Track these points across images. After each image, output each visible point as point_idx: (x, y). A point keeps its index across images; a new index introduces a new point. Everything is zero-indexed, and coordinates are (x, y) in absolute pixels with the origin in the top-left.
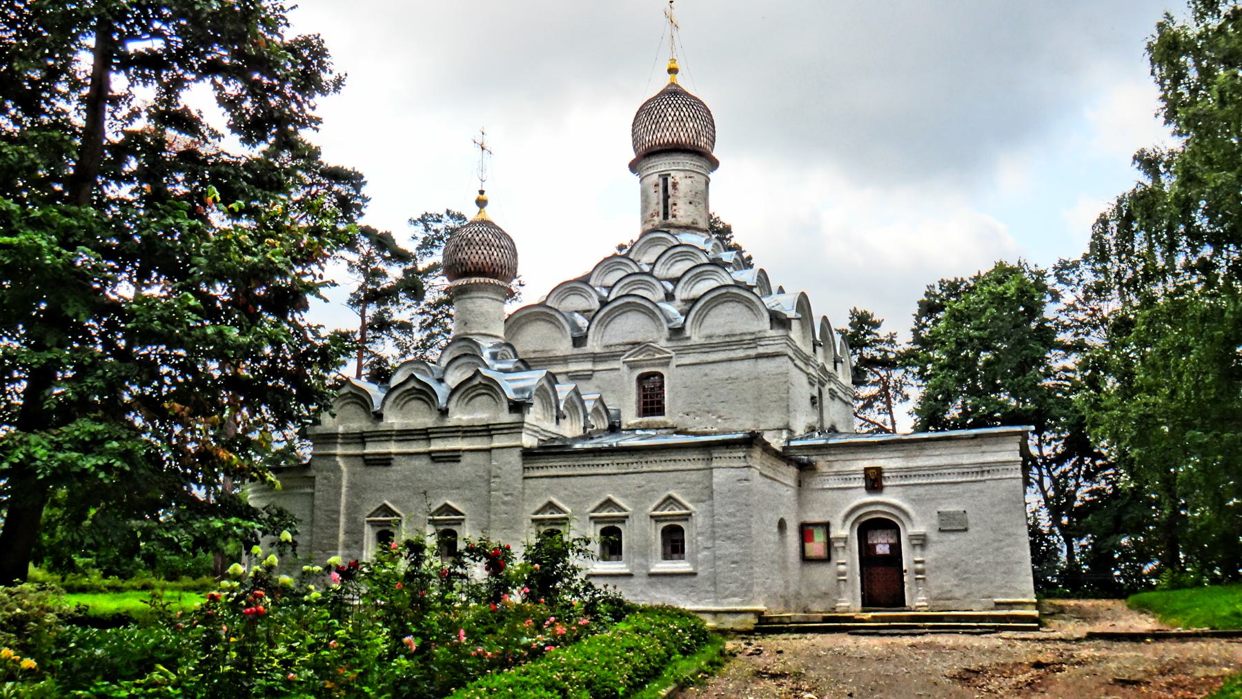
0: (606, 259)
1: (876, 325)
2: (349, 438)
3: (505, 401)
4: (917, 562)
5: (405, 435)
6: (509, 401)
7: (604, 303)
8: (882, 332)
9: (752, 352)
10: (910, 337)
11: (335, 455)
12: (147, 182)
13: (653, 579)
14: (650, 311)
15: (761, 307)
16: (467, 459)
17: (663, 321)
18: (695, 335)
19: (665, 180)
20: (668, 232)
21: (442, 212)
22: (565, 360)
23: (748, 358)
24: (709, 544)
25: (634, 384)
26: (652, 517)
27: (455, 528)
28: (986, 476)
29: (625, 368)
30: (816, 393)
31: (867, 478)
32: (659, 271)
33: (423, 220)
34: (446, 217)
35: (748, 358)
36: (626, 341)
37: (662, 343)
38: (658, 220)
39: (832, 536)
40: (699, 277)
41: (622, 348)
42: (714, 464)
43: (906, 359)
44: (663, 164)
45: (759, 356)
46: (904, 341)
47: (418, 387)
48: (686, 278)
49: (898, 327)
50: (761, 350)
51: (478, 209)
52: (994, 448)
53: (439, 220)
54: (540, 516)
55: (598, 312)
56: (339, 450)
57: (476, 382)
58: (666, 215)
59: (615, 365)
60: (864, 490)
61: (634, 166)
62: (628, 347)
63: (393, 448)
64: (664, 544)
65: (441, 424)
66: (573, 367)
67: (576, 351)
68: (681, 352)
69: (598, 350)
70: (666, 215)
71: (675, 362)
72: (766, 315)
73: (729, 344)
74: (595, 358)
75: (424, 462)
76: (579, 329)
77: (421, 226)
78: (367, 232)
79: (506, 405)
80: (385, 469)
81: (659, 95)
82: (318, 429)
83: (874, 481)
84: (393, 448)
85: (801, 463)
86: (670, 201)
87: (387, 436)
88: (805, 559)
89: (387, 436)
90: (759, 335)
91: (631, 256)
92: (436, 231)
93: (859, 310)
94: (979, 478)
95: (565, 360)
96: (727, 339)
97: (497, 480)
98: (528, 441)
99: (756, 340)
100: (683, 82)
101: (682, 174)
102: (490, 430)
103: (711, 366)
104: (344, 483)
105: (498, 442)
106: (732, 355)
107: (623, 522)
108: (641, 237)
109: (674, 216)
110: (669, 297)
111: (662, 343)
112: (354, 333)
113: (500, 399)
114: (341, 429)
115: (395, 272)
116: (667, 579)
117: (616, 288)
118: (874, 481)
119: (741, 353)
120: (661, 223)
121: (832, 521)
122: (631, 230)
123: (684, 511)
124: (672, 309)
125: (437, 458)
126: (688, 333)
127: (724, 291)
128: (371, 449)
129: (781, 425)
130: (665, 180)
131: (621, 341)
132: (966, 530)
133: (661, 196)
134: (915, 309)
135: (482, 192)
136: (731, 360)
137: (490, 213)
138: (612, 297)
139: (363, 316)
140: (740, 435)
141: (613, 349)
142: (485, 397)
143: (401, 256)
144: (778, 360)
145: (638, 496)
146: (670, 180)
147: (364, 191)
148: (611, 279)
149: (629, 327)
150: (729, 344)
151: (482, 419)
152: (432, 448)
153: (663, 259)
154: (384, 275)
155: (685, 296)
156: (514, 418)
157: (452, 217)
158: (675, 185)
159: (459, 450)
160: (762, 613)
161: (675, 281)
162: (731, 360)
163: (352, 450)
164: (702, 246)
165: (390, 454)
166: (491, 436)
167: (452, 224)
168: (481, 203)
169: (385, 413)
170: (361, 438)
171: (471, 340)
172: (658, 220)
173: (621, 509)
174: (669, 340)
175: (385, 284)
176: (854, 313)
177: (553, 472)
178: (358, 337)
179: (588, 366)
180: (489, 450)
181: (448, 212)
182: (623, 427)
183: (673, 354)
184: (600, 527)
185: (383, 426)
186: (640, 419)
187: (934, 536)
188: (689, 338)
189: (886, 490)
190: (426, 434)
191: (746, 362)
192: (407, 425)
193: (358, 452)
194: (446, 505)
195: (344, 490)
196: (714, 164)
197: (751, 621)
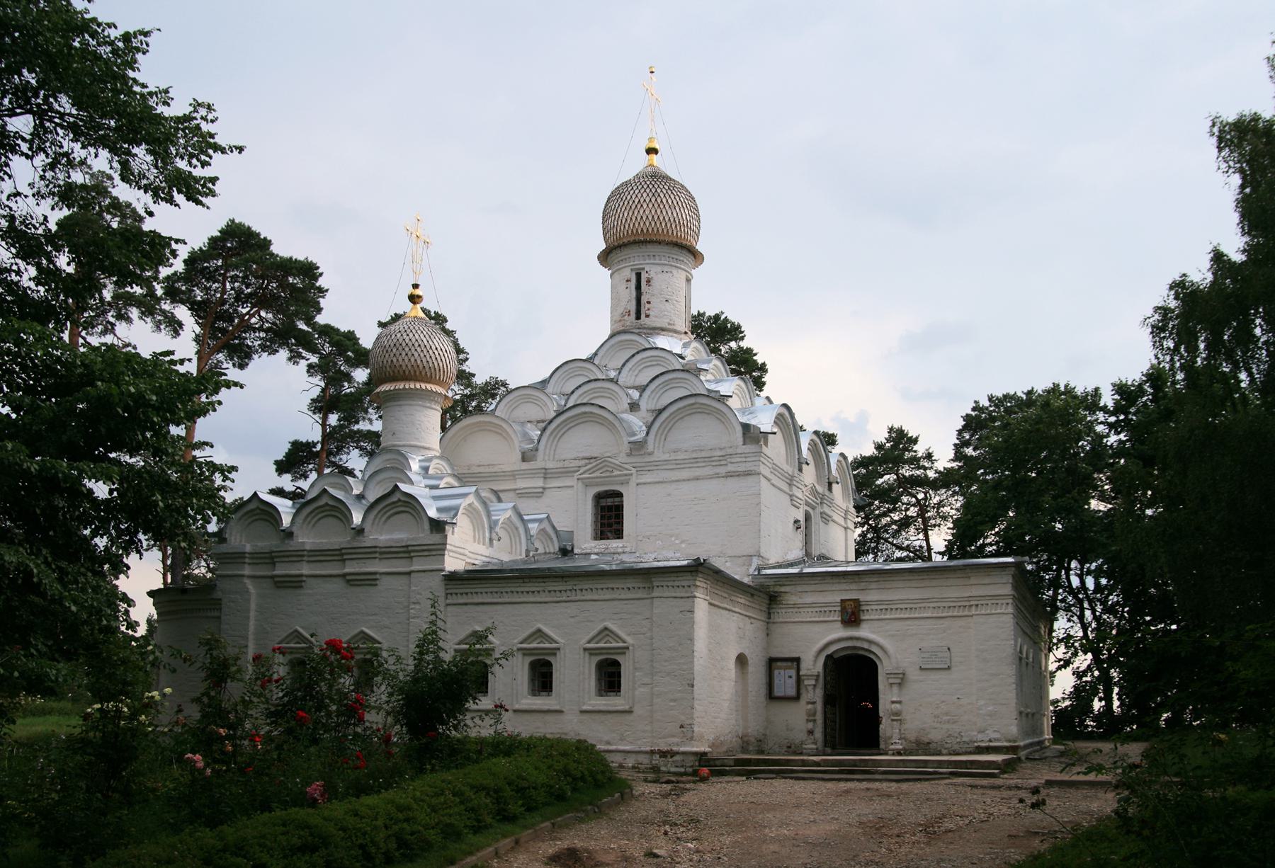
0: (566, 363)
1: (915, 441)
3: (425, 520)
4: (893, 702)
5: (319, 555)
6: (430, 519)
8: (920, 449)
9: (722, 470)
10: (951, 455)
11: (243, 576)
12: (1254, 336)
13: (585, 717)
14: (607, 421)
15: (733, 420)
16: (385, 582)
17: (623, 433)
19: (639, 276)
20: (639, 334)
22: (513, 475)
23: (717, 476)
24: (646, 680)
26: (585, 649)
30: (801, 518)
31: (843, 611)
32: (625, 378)
36: (582, 455)
40: (667, 386)
41: (577, 463)
42: (655, 594)
43: (946, 480)
44: (635, 259)
45: (730, 475)
46: (944, 459)
47: (331, 503)
48: (653, 386)
49: (939, 444)
50: (731, 468)
52: (987, 581)
55: (551, 422)
56: (247, 571)
57: (394, 498)
58: (638, 317)
59: (568, 482)
60: (839, 625)
61: (605, 258)
62: (583, 462)
63: (305, 570)
64: (599, 680)
65: (356, 544)
66: (521, 484)
67: (525, 466)
68: (640, 469)
69: (550, 465)
70: (638, 317)
71: (634, 480)
72: (739, 429)
74: (546, 474)
75: (338, 585)
76: (531, 441)
78: (327, 331)
79: (427, 526)
80: (298, 591)
82: (224, 548)
83: (852, 615)
84: (305, 570)
85: (767, 595)
86: (644, 299)
87: (299, 556)
88: (771, 696)
90: (730, 451)
91: (596, 361)
93: (896, 426)
94: (966, 613)
95: (513, 475)
96: (694, 455)
97: (417, 607)
99: (725, 458)
101: (659, 269)
102: (272, 558)
103: (674, 486)
104: (253, 606)
106: (698, 472)
107: (555, 654)
109: (647, 316)
110: (634, 407)
111: (622, 458)
112: (314, 445)
113: (421, 518)
114: (248, 548)
116: (597, 717)
117: (577, 396)
118: (852, 615)
119: (708, 471)
121: (803, 657)
123: (621, 644)
124: (637, 422)
125: (352, 581)
126: (650, 447)
127: (692, 401)
129: (751, 551)
131: (575, 455)
132: (949, 668)
134: (960, 423)
138: (570, 404)
139: (324, 425)
140: (685, 563)
141: (567, 464)
142: (403, 516)
144: (750, 479)
145: (571, 628)
147: (321, 282)
149: (582, 442)
151: (402, 540)
152: (347, 570)
153: (629, 365)
154: (348, 377)
156: (436, 538)
158: (648, 281)
159: (375, 573)
160: (705, 754)
162: (466, 604)
163: (264, 571)
164: (677, 350)
165: (301, 575)
166: (411, 558)
168: (414, 299)
169: (367, 527)
170: (270, 558)
171: (399, 452)
173: (552, 641)
174: (629, 455)
175: (347, 389)
176: (891, 430)
178: (319, 447)
179: (540, 483)
180: (409, 573)
182: (576, 551)
183: (634, 471)
184: (529, 659)
185: (292, 545)
187: (913, 674)
188: (650, 454)
189: (864, 625)
190: (340, 555)
191: (715, 482)
192: (392, 540)
193: (269, 574)
194: (362, 632)
195: (252, 614)
196: (696, 256)
197: (690, 761)
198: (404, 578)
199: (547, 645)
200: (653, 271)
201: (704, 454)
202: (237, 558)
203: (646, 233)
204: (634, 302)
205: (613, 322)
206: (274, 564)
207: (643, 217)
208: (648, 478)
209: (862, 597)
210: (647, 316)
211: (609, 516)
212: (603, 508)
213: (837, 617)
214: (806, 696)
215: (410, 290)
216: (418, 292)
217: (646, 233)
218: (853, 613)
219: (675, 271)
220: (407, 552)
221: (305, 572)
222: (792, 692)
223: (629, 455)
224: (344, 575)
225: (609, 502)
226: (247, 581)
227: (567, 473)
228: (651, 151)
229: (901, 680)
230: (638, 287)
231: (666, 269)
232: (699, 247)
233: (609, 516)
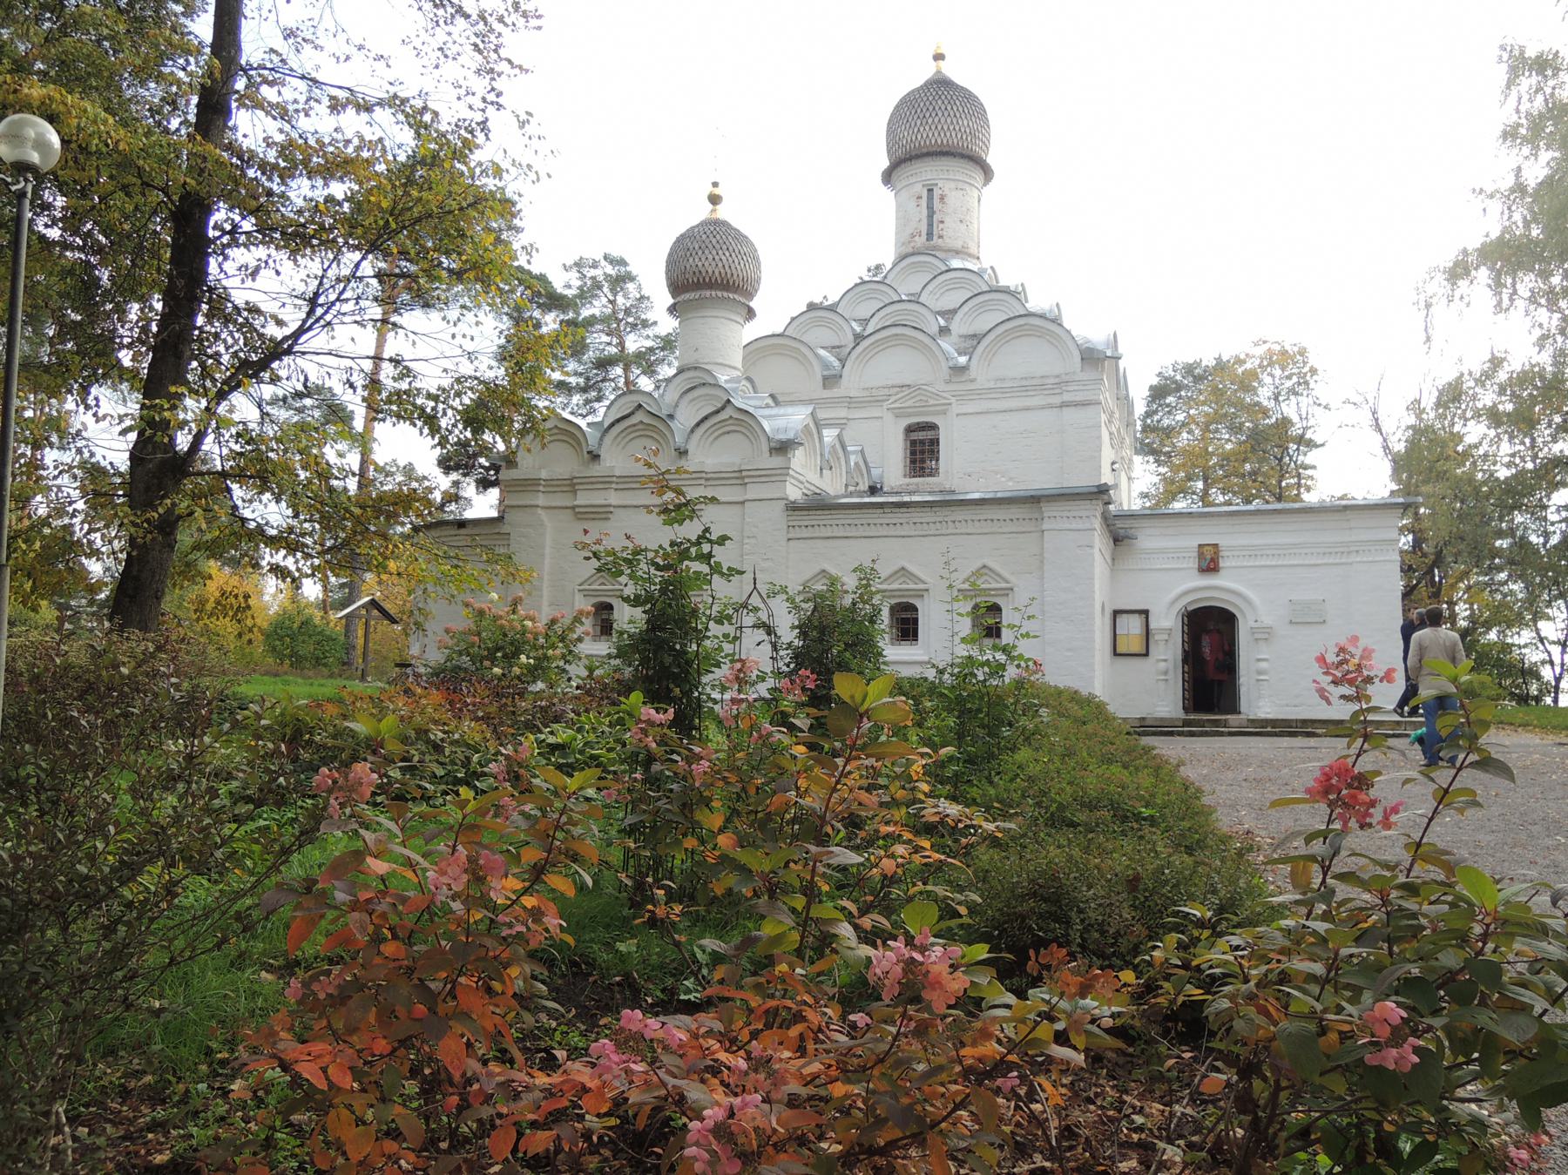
0: (793, 319)
2: (553, 485)
7: (858, 338)
9: (1057, 400)
17: (941, 358)
18: (981, 373)
19: (930, 191)
21: (599, 257)
23: (1051, 406)
25: (901, 436)
27: (999, 601)
28: (1353, 558)
29: (889, 417)
31: (1201, 555)
33: (579, 265)
34: (603, 263)
35: (1051, 406)
36: (890, 383)
37: (940, 386)
38: (921, 241)
39: (1152, 626)
41: (886, 391)
42: (1045, 527)
44: (928, 171)
47: (647, 420)
48: (966, 308)
50: (1067, 397)
51: (711, 206)
53: (595, 265)
54: (586, 587)
56: (541, 500)
59: (876, 412)
61: (888, 177)
63: (614, 498)
67: (827, 394)
70: (930, 235)
71: (956, 408)
72: (1077, 354)
73: (1025, 388)
74: (851, 403)
77: (574, 274)
81: (925, 84)
83: (1209, 563)
84: (614, 498)
87: (606, 482)
88: (1116, 654)
89: (606, 482)
90: (1065, 378)
92: (593, 278)
96: (1024, 383)
97: (753, 541)
98: (794, 493)
99: (1061, 383)
100: (951, 71)
101: (952, 185)
104: (548, 542)
105: (753, 492)
108: (894, 265)
109: (940, 237)
111: (940, 386)
114: (544, 474)
115: (550, 322)
117: (846, 332)
118: (1209, 563)
120: (927, 244)
122: (886, 255)
123: (1004, 585)
126: (973, 373)
128: (583, 499)
130: (930, 191)
133: (925, 212)
135: (715, 185)
136: (1027, 409)
137: (723, 212)
138: (870, 330)
141: (875, 392)
142: (740, 436)
143: (554, 301)
146: (937, 192)
148: (865, 310)
150: (1025, 388)
153: (930, 287)
155: (965, 330)
156: (777, 461)
157: (611, 262)
158: (942, 198)
161: (949, 314)
162: (1027, 409)
167: (610, 270)
169: (691, 448)
170: (571, 485)
172: (921, 241)
177: (828, 532)
179: (843, 413)
180: (743, 503)
181: (606, 258)
183: (953, 400)
186: (908, 480)
189: (1222, 572)
193: (569, 504)
195: (548, 551)
198: (737, 508)
199: (912, 586)
200: (945, 187)
201: (1034, 382)
202: (530, 484)
203: (936, 136)
204: (925, 221)
205: (899, 243)
206: (575, 492)
207: (709, 265)
208: (969, 408)
209: (1223, 542)
210: (940, 237)
211: (922, 449)
212: (913, 443)
213: (1194, 564)
214: (1158, 651)
215: (710, 189)
216: (717, 191)
217: (936, 136)
218: (1212, 560)
219: (967, 187)
220: (740, 477)
221: (613, 501)
222: (1137, 647)
223: (948, 382)
224: (573, 508)
225: (921, 435)
226: (539, 511)
227: (877, 402)
228: (939, 57)
229: (1265, 635)
230: (930, 208)
231: (960, 185)
232: (990, 160)
233: (922, 449)
